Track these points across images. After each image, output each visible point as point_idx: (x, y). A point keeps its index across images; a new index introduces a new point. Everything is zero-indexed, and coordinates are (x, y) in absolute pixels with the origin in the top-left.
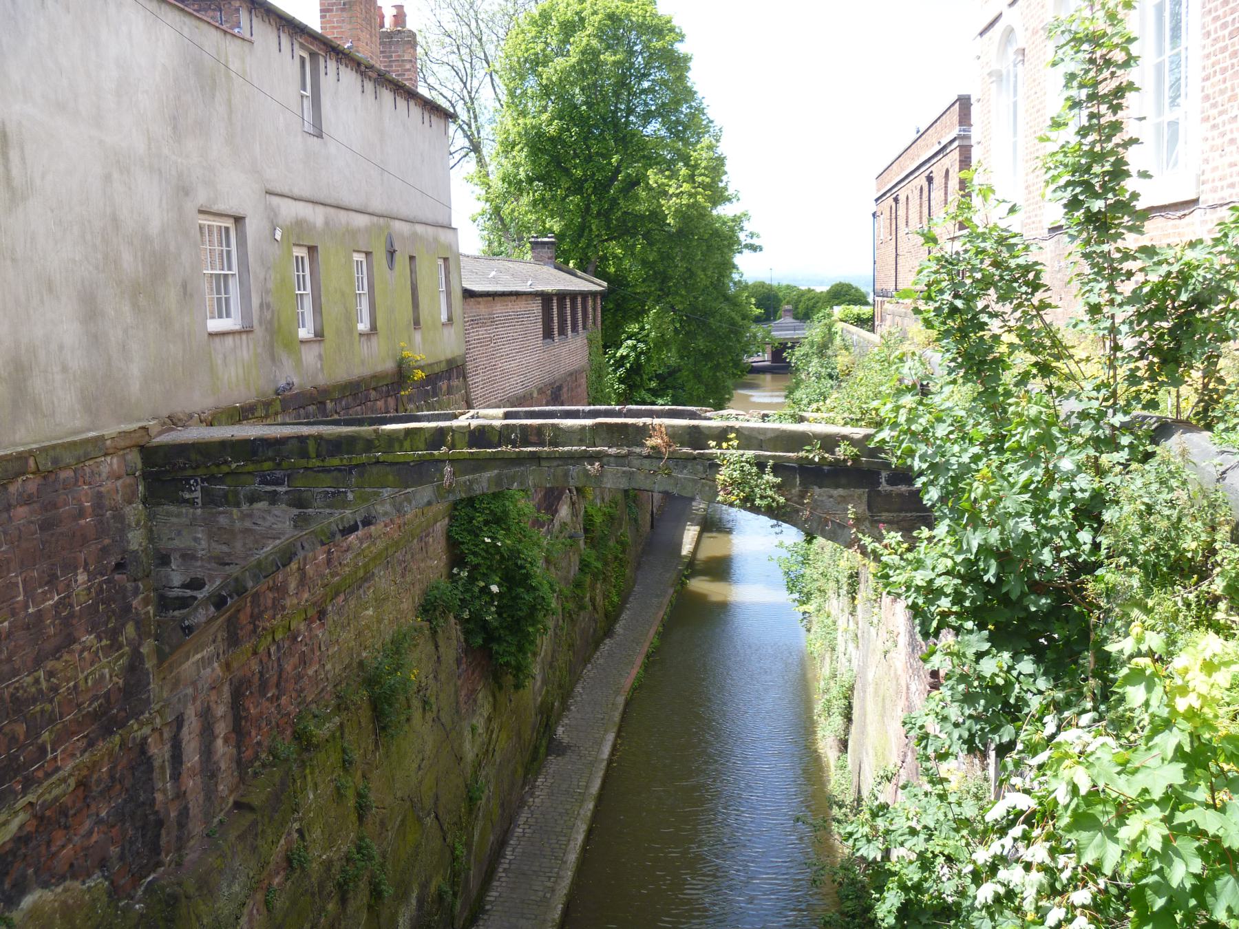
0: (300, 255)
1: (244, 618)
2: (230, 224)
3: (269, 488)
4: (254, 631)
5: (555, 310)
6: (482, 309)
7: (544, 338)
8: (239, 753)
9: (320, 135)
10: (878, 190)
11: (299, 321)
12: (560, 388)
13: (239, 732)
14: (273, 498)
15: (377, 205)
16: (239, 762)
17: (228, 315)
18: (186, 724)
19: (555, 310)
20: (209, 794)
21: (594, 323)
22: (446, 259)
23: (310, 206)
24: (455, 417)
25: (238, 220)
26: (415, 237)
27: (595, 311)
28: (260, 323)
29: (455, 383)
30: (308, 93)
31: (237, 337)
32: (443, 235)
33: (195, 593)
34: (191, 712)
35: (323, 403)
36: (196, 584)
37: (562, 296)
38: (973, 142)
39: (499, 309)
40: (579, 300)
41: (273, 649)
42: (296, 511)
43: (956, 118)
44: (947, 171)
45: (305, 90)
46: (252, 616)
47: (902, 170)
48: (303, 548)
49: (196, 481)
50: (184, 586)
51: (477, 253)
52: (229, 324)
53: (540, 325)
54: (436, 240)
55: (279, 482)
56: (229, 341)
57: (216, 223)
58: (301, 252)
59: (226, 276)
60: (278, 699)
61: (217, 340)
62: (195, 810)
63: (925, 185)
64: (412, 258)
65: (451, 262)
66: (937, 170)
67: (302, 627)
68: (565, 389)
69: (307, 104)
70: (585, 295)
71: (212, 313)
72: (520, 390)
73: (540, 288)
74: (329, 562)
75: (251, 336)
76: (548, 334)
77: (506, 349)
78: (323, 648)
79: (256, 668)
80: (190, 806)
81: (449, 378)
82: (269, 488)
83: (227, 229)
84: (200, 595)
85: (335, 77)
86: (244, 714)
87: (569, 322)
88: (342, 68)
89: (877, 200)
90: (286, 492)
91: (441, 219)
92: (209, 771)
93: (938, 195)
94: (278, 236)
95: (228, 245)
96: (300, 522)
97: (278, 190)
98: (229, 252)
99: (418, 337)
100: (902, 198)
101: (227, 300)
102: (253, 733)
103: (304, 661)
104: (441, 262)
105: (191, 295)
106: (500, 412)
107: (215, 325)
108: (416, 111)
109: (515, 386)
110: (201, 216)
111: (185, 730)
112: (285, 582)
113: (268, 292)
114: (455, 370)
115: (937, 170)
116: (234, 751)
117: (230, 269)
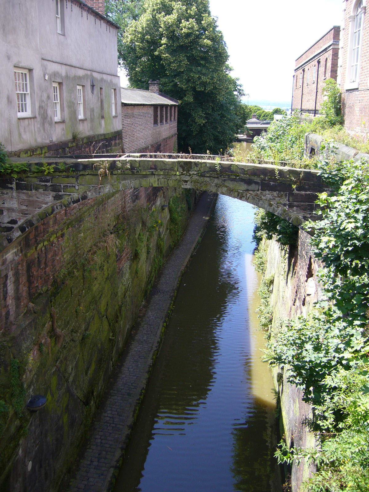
0: (55, 86)
1: (31, 236)
2: (26, 72)
3: (43, 184)
4: (36, 241)
5: (159, 112)
6: (129, 110)
7: (154, 124)
8: (29, 290)
9: (64, 35)
10: (296, 66)
11: (55, 113)
12: (160, 145)
13: (30, 282)
14: (46, 188)
15: (87, 65)
16: (29, 293)
17: (26, 111)
18: (9, 278)
19: (159, 112)
20: (18, 306)
21: (174, 119)
22: (115, 90)
23: (59, 65)
24: (120, 156)
25: (30, 70)
26: (102, 79)
27: (175, 114)
28: (39, 114)
29: (117, 141)
30: (59, 16)
31: (30, 120)
32: (114, 80)
33: (13, 226)
34: (11, 274)
35: (64, 149)
36: (14, 222)
37: (162, 106)
38: (340, 46)
39: (136, 111)
40: (169, 108)
41: (43, 249)
42: (55, 193)
43: (332, 36)
44: (327, 59)
45: (58, 15)
46: (35, 235)
47: (307, 58)
48: (57, 208)
49: (14, 180)
50: (8, 223)
51: (126, 87)
52: (28, 113)
53: (152, 118)
54: (111, 81)
55: (47, 181)
56: (26, 121)
57: (21, 71)
58: (56, 85)
59: (25, 94)
60: (45, 269)
61: (21, 121)
62: (12, 313)
63: (317, 64)
64: (101, 88)
65: (117, 91)
66: (322, 59)
67: (55, 240)
68: (162, 145)
69: (59, 21)
70: (172, 106)
71: (19, 109)
72: (144, 146)
73: (153, 103)
74: (66, 213)
75: (35, 119)
76: (155, 122)
77: (139, 128)
78: (63, 249)
79: (36, 256)
80: (10, 311)
81: (112, 141)
82: (43, 184)
83: (25, 74)
84: (15, 226)
85: (71, 10)
86: (31, 275)
87: (164, 117)
88: (73, 5)
89: (295, 70)
90: (51, 186)
91: (113, 73)
92: (18, 298)
93: (322, 69)
94: (47, 78)
95: (26, 81)
96: (57, 197)
97: (47, 59)
98: (26, 84)
99: (103, 122)
100: (306, 70)
101: (25, 104)
102: (35, 282)
103: (55, 254)
104: (113, 90)
105: (11, 102)
106: (139, 154)
107: (21, 115)
108: (104, 25)
109: (142, 143)
110: (16, 68)
111: (8, 281)
112: (48, 223)
113: (43, 101)
114: (118, 135)
115: (322, 59)
116: (28, 289)
117: (26, 91)
